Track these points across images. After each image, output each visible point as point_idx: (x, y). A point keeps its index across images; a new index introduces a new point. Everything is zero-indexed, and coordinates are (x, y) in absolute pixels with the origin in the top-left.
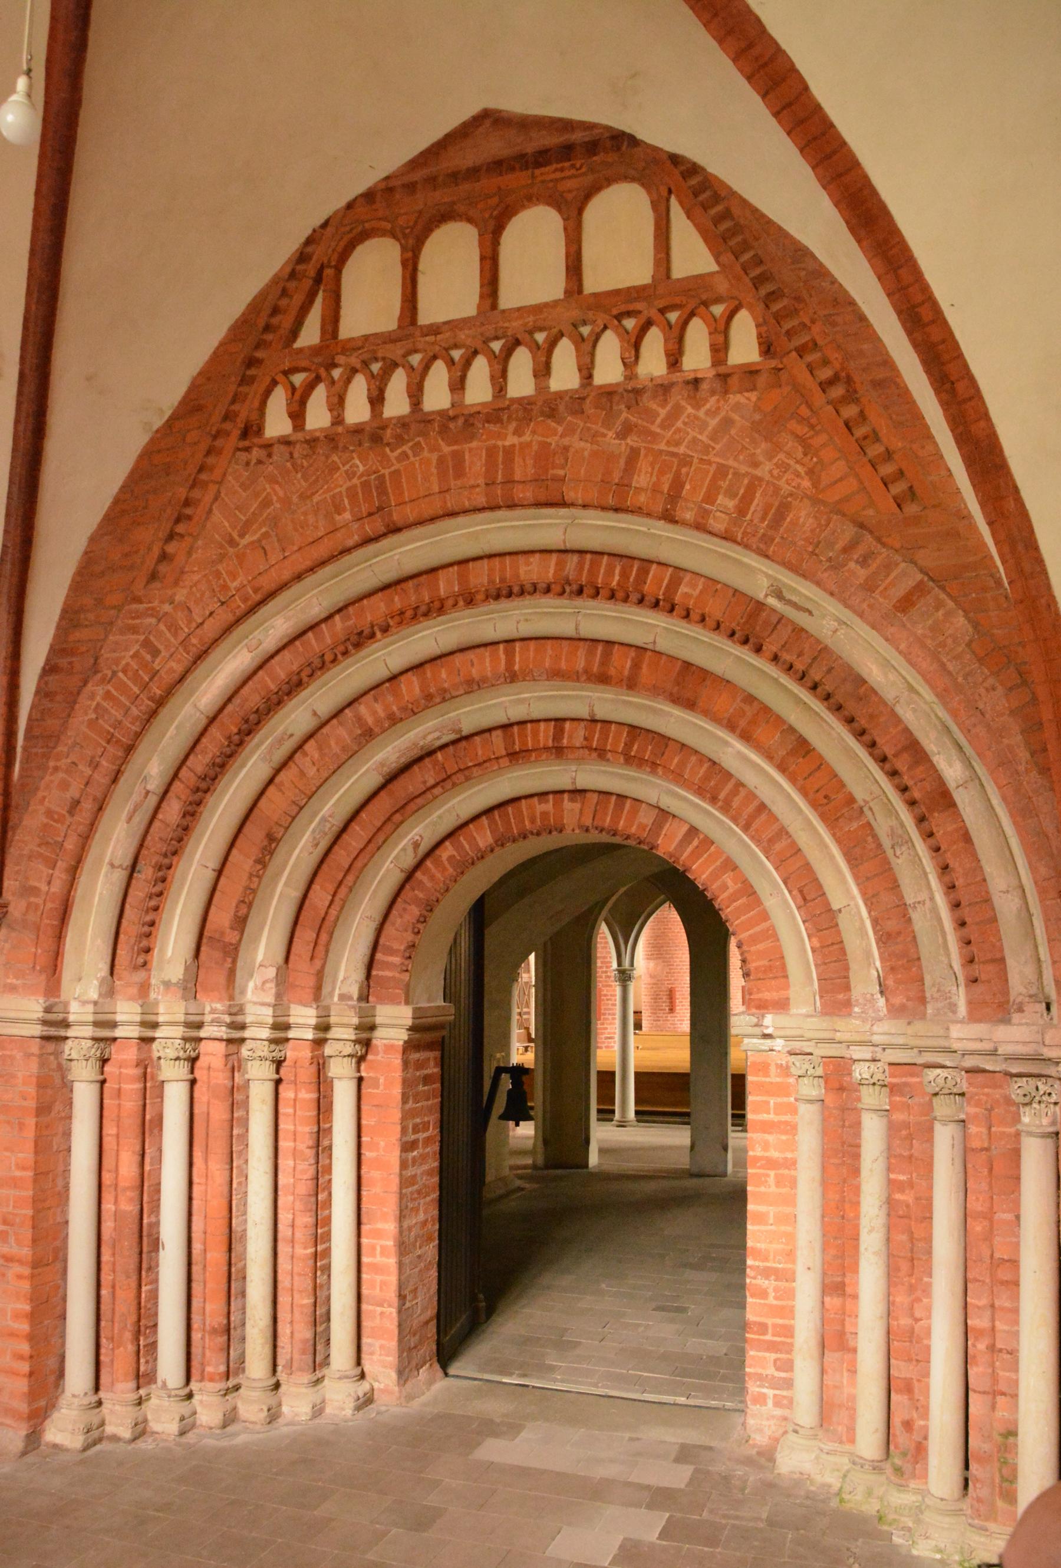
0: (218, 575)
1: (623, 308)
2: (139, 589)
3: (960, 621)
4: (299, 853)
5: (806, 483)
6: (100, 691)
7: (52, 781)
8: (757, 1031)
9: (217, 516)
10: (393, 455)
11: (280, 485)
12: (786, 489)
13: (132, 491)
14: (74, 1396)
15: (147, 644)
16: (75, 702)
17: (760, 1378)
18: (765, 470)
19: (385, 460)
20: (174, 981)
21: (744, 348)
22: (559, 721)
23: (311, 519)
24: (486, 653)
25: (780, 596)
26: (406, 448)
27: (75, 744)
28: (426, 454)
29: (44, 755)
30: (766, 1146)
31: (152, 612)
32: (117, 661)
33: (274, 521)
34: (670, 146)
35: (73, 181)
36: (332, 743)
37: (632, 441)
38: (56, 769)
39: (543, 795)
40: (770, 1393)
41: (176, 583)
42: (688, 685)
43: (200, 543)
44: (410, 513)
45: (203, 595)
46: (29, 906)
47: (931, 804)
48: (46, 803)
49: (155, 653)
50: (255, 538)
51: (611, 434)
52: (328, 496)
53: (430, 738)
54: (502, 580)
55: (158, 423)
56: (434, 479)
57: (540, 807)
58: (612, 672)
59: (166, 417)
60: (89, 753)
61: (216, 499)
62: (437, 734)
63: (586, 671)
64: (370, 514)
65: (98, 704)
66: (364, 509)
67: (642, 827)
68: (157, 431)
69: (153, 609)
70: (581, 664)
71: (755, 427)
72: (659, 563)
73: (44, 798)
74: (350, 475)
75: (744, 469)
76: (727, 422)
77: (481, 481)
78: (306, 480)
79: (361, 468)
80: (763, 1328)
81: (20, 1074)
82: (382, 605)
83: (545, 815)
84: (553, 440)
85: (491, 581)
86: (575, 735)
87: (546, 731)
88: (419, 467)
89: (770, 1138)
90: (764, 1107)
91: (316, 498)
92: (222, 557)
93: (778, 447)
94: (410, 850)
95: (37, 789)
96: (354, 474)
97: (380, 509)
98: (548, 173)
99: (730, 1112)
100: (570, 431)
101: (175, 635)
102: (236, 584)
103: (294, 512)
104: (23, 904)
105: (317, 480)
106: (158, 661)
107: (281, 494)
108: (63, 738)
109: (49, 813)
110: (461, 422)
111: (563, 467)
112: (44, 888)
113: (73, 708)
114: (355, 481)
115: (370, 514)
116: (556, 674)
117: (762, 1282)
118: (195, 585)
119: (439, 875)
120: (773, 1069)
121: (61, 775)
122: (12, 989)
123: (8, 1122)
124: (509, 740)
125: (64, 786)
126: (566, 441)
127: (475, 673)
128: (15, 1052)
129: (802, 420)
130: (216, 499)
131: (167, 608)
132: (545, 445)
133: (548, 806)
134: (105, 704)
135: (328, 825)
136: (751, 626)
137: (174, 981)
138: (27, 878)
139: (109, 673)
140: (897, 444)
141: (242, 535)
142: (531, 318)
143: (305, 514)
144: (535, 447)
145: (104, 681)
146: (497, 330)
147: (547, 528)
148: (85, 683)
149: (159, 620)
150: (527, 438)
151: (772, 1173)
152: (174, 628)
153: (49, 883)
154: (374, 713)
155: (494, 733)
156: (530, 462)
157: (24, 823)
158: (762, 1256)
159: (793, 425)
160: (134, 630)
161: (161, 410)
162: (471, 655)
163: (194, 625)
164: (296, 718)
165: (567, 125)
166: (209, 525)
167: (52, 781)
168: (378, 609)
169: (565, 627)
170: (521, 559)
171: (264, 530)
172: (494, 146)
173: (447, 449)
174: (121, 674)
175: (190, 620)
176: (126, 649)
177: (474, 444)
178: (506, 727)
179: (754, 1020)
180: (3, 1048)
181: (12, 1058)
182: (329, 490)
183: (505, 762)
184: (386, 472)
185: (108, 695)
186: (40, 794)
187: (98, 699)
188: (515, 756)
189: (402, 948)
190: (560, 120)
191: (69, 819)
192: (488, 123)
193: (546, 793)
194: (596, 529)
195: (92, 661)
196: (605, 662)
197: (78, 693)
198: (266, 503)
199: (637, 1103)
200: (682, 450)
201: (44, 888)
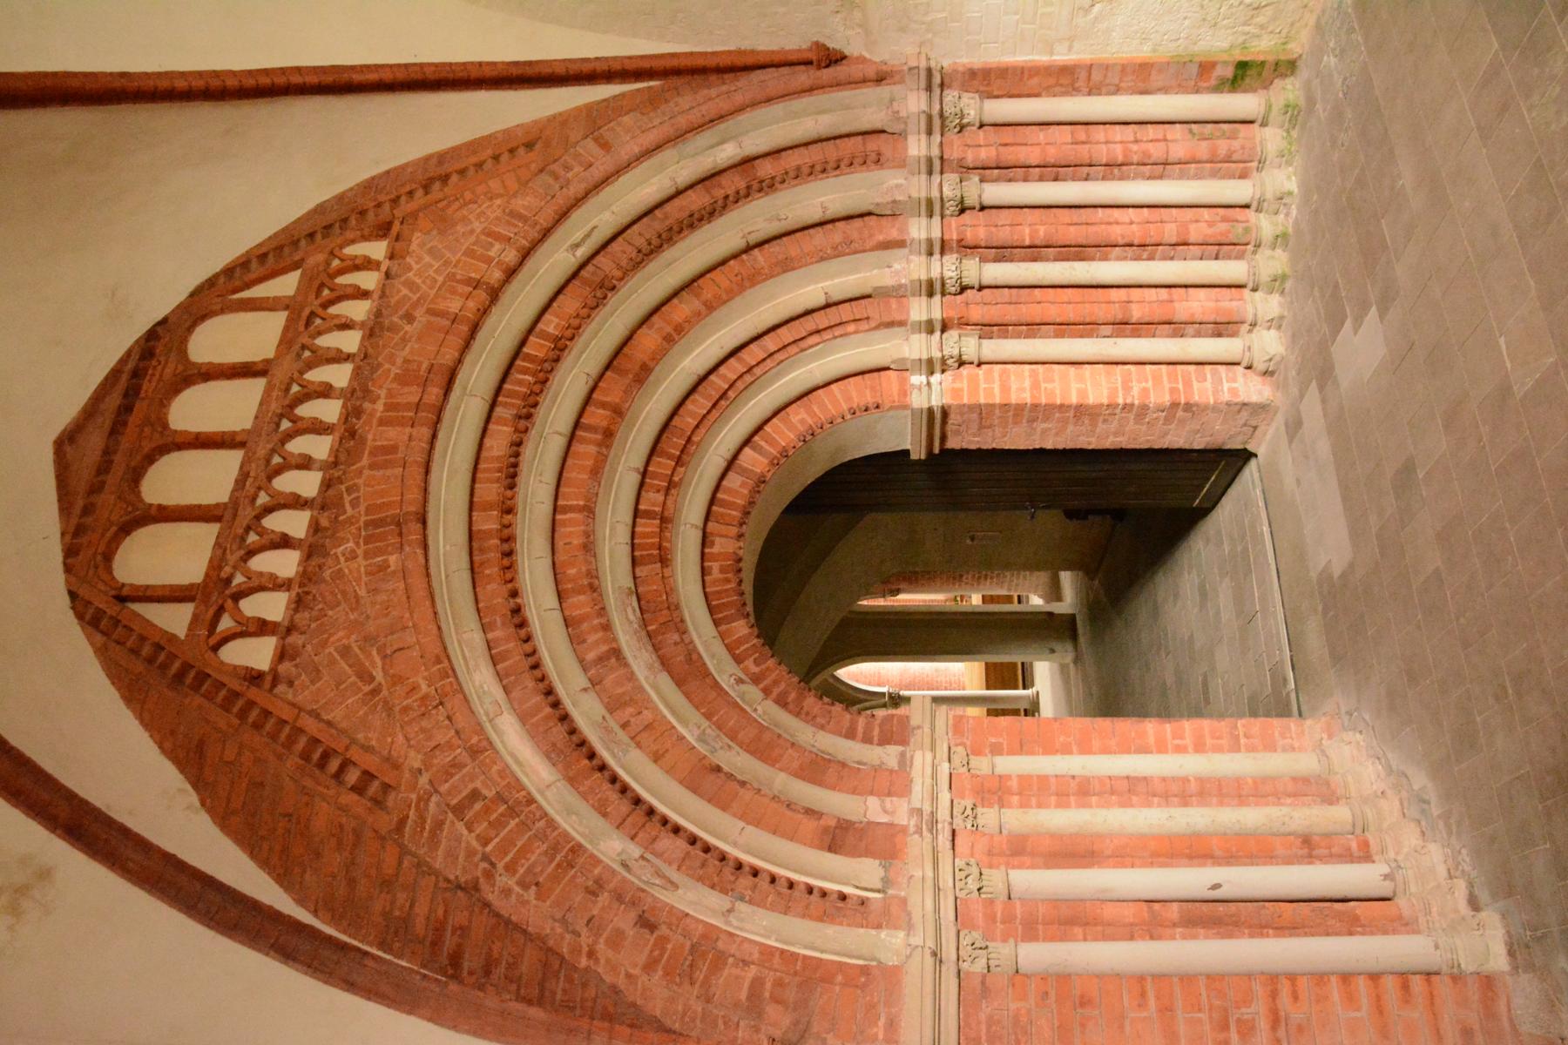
0: (405, 710)
1: (276, 438)
2: (385, 822)
3: (626, 119)
4: (737, 760)
5: (498, 202)
6: (503, 880)
7: (608, 961)
8: (925, 389)
9: (336, 715)
10: (350, 511)
11: (331, 635)
12: (498, 213)
13: (263, 838)
14: (1437, 947)
15: (459, 810)
16: (508, 922)
17: (1216, 392)
18: (478, 226)
19: (350, 521)
20: (881, 873)
21: (376, 249)
22: (637, 513)
23: (382, 597)
24: (561, 530)
25: (577, 246)
26: (347, 499)
27: (563, 921)
28: (360, 481)
29: (569, 980)
30: (1022, 390)
31: (424, 799)
32: (471, 853)
33: (369, 639)
34: (181, 296)
35: (109, 107)
36: (620, 691)
37: (419, 313)
38: (591, 954)
39: (704, 572)
40: (1226, 386)
41: (397, 767)
42: (627, 366)
43: (360, 736)
44: (414, 495)
45: (423, 730)
46: (776, 1000)
47: (750, 177)
48: (636, 971)
49: (475, 795)
50: (379, 663)
51: (408, 328)
52: (364, 579)
53: (631, 617)
54: (500, 470)
55: (194, 798)
56: (389, 472)
57: (716, 573)
58: (605, 423)
59: (189, 787)
60: (579, 897)
61: (317, 716)
62: (629, 610)
63: (599, 445)
64: (400, 534)
65: (518, 883)
66: (394, 540)
67: (743, 485)
68: (203, 804)
69: (419, 799)
70: (592, 449)
71: (442, 232)
72: (490, 649)
73: (629, 976)
74: (352, 556)
75: (472, 239)
76: (431, 252)
77: (408, 430)
78: (338, 604)
79: (351, 544)
80: (1173, 391)
81: (1013, 1006)
82: (489, 587)
83: (722, 571)
84: (395, 370)
85: (498, 480)
86: (652, 500)
87: (645, 525)
88: (373, 485)
89: (1014, 387)
90: (989, 392)
91: (362, 592)
92: (389, 709)
93: (464, 219)
94: (744, 687)
95: (615, 989)
96: (353, 551)
97: (399, 524)
98: (147, 386)
99: (1020, 692)
100: (391, 359)
101: (461, 766)
102: (424, 687)
103: (368, 617)
104: (772, 1011)
105: (344, 593)
106: (485, 792)
107: (341, 634)
108: (551, 943)
109: (649, 967)
110: (349, 433)
111: (420, 364)
112: (753, 971)
113: (517, 927)
114: (360, 552)
115: (400, 534)
116: (596, 472)
117: (1136, 391)
118: (408, 740)
119: (773, 676)
120: (957, 385)
121: (601, 946)
122: (892, 1025)
123: (1083, 1025)
124: (648, 560)
125: (616, 940)
126: (399, 361)
127: (577, 541)
128: (983, 1017)
129: (448, 206)
130: (317, 716)
131: (423, 780)
132: (397, 378)
133: (715, 567)
134: (521, 871)
135: (709, 731)
136: (591, 283)
137: (881, 873)
138: (737, 1005)
139: (484, 865)
140: (489, 152)
141: (372, 678)
142: (275, 394)
143: (373, 603)
144: (394, 385)
145: (489, 875)
146: (261, 451)
147: (467, 409)
148: (487, 905)
149: (436, 791)
150: (383, 393)
151: (1043, 385)
152: (456, 765)
153: (746, 963)
154: (597, 643)
155: (638, 573)
156: (406, 389)
157: (658, 1013)
158: (1113, 392)
159: (449, 211)
160: (439, 825)
161: (180, 790)
162: (560, 544)
163: (456, 741)
164: (587, 712)
165: (115, 373)
166: (344, 725)
167: (608, 961)
168: (494, 591)
169: (556, 445)
170: (484, 454)
171: (374, 652)
172: (94, 441)
173: (365, 461)
174: (489, 848)
175: (450, 746)
176: (458, 840)
177: (370, 437)
178: (634, 562)
179: (915, 392)
180: (977, 1040)
181: (991, 1021)
182: (358, 580)
183: (667, 572)
184: (363, 519)
185: (510, 868)
186: (621, 982)
187: (512, 882)
188: (664, 560)
189: (848, 716)
190: (106, 378)
191: (664, 930)
192: (68, 449)
193: (703, 568)
194: (479, 374)
195: (460, 893)
196: (595, 426)
197: (498, 915)
198: (345, 652)
199: (1016, 688)
200: (440, 279)
201: (753, 971)
